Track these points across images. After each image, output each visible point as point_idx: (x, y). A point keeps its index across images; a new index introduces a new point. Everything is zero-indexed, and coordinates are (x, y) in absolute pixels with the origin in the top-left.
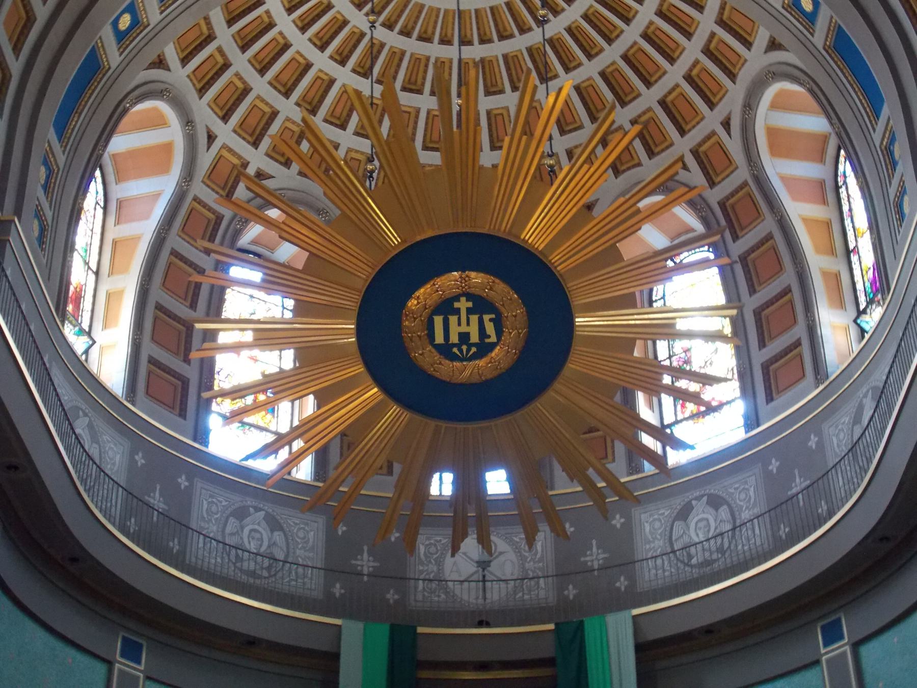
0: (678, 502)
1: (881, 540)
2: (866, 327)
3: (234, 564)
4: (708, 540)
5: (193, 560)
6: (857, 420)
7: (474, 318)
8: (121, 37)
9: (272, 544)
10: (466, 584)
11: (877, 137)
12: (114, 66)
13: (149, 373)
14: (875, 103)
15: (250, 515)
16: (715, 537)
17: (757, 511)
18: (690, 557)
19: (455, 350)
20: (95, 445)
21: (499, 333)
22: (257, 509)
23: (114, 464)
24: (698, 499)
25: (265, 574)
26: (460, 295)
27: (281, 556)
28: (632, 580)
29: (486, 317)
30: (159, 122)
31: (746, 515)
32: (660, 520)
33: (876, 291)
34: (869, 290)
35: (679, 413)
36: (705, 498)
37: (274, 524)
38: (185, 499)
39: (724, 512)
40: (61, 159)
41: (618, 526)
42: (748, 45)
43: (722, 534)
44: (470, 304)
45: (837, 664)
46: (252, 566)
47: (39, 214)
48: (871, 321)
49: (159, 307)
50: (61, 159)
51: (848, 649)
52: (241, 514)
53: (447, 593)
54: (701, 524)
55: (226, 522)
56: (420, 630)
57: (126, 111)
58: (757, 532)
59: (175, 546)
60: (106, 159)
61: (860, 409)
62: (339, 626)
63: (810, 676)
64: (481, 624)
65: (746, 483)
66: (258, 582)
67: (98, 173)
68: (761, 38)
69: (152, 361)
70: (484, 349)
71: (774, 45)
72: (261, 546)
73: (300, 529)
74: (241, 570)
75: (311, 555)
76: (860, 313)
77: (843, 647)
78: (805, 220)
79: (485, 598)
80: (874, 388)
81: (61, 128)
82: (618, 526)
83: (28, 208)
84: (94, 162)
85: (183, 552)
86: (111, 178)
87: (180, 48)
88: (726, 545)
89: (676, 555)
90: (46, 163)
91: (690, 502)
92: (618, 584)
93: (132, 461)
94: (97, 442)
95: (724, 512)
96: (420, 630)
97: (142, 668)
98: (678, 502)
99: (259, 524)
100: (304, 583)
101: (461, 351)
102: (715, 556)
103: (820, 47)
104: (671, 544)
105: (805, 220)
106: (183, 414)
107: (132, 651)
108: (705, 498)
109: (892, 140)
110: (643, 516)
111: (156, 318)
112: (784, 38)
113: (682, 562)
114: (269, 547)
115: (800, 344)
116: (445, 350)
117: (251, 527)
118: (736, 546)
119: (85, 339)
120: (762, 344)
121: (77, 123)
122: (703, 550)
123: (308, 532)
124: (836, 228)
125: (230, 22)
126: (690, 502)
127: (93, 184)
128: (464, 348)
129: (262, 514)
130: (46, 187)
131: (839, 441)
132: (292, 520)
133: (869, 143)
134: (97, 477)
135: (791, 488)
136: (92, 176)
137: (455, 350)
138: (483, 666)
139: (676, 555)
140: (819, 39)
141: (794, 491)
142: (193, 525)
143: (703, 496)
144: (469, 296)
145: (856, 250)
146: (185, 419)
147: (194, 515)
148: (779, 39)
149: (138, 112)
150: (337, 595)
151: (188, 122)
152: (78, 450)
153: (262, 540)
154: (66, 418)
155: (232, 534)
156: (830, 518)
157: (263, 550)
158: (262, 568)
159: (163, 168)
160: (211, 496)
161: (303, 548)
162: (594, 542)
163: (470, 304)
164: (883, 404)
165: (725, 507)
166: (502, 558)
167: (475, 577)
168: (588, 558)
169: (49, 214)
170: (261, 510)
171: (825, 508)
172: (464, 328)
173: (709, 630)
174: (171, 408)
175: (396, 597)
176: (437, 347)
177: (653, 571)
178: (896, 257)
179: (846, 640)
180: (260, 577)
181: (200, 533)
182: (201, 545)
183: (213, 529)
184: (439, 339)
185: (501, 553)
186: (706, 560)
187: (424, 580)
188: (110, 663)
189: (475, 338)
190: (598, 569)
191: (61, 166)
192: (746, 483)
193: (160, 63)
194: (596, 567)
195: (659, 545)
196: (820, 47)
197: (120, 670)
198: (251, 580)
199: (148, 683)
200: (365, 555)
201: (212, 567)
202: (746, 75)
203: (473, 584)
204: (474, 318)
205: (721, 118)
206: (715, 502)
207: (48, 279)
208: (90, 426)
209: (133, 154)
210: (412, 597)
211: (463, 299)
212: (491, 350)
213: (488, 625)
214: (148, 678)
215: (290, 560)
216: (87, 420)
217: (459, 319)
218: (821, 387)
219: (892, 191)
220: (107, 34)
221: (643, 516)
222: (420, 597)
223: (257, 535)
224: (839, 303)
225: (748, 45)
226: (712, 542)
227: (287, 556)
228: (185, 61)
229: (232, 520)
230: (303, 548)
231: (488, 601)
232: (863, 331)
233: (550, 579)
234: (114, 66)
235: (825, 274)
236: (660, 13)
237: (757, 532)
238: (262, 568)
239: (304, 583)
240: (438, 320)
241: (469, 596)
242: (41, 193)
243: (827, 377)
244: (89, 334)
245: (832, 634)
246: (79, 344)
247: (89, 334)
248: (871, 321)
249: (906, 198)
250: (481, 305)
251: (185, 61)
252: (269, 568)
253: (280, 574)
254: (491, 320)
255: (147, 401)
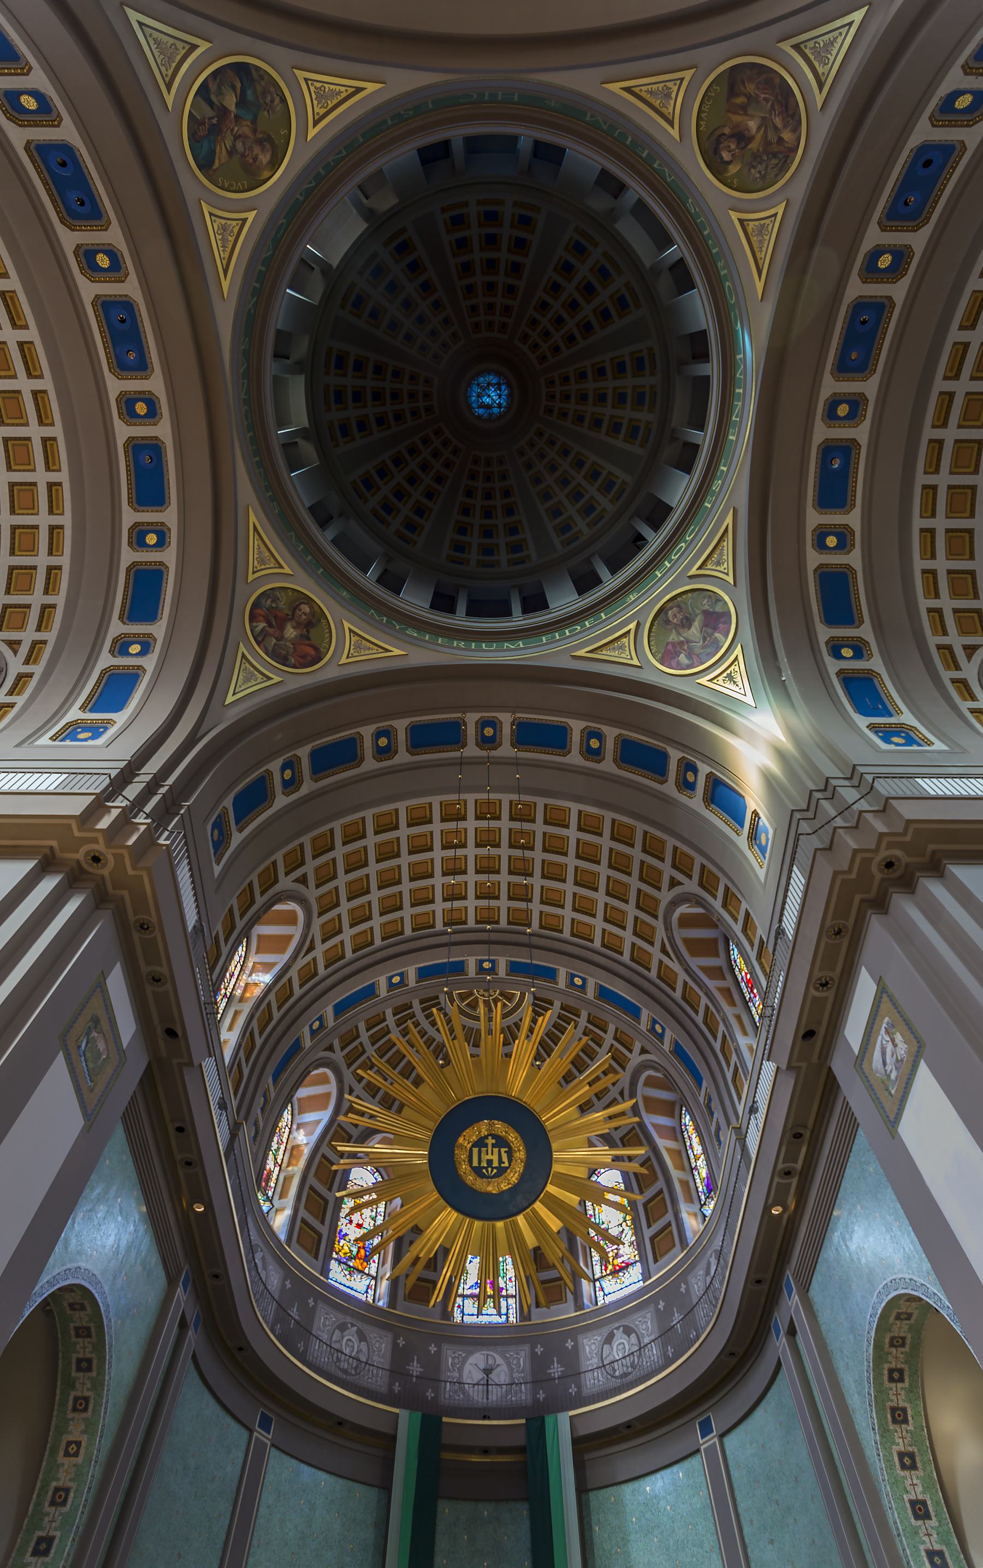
0: (605, 1331)
1: (730, 1354)
2: (707, 1215)
3: (335, 1363)
4: (624, 1358)
5: (311, 1358)
6: (708, 1273)
7: (496, 1150)
8: (313, 1033)
9: (359, 1351)
10: (476, 1386)
11: (701, 1099)
12: (307, 1047)
13: (301, 1228)
14: (698, 1080)
15: (348, 1328)
16: (628, 1355)
17: (653, 1337)
18: (614, 1371)
19: (484, 1171)
20: (264, 1272)
21: (510, 1161)
22: (353, 1325)
23: (273, 1286)
24: (618, 1328)
25: (353, 1372)
26: (488, 1135)
27: (364, 1359)
28: (579, 1387)
29: (503, 1150)
30: (324, 1080)
31: (646, 1340)
32: (594, 1343)
33: (710, 1191)
34: (706, 1191)
35: (604, 1271)
36: (622, 1328)
37: (362, 1337)
38: (310, 1314)
39: (633, 1338)
40: (273, 1095)
41: (570, 1347)
42: (631, 1051)
43: (633, 1353)
44: (494, 1141)
45: (711, 1451)
46: (346, 1367)
47: (256, 1124)
48: (708, 1210)
49: (311, 1188)
50: (273, 1095)
51: (716, 1440)
52: (342, 1328)
53: (464, 1394)
54: (620, 1347)
55: (334, 1332)
56: (445, 1419)
57: (310, 1072)
58: (655, 1352)
59: (301, 1346)
60: (295, 1099)
61: (709, 1264)
62: (398, 1414)
63: (697, 1457)
64: (485, 1418)
65: (646, 1317)
66: (349, 1377)
67: (290, 1105)
68: (637, 1047)
69: (304, 1221)
70: (501, 1171)
71: (644, 1051)
72: (353, 1351)
73: (377, 1341)
74: (339, 1368)
75: (382, 1360)
76: (702, 1206)
77: (713, 1439)
78: (668, 1150)
79: (488, 1399)
80: (716, 1251)
81: (276, 1077)
82: (570, 1347)
83: (251, 1120)
84: (289, 1100)
85: (305, 1351)
86: (296, 1111)
87: (341, 1041)
88: (636, 1362)
89: (605, 1369)
90: (265, 1096)
91: (612, 1331)
92: (570, 1391)
93: (284, 1285)
94: (266, 1270)
95: (633, 1338)
96: (445, 1419)
97: (270, 1437)
98: (605, 1331)
99: (353, 1336)
100: (376, 1381)
101: (487, 1171)
102: (630, 1370)
103: (667, 1051)
104: (603, 1361)
105: (668, 1150)
106: (316, 1257)
107: (265, 1424)
108: (622, 1328)
109: (710, 1100)
110: (585, 1341)
111: (309, 1195)
112: (648, 1047)
113: (610, 1375)
114: (357, 1352)
115: (671, 1225)
116: (478, 1171)
117: (347, 1338)
118: (643, 1362)
119: (268, 1204)
120: (649, 1226)
121: (284, 1076)
122: (623, 1365)
123: (382, 1344)
124: (684, 1155)
125: (368, 1030)
126: (612, 1331)
127: (286, 1112)
128: (490, 1169)
129: (356, 1328)
130: (262, 1109)
131: (699, 1287)
132: (373, 1333)
133: (697, 1101)
134: (262, 1293)
135: (673, 1321)
136: (286, 1107)
137: (484, 1171)
138: (486, 1451)
139: (605, 1369)
140: (666, 1047)
141: (675, 1323)
142: (314, 1333)
143: (620, 1326)
144: (494, 1136)
145: (696, 1168)
146: (317, 1260)
147: (315, 1326)
148: (646, 1048)
149: (314, 1075)
150: (396, 1391)
151: (340, 1081)
152: (254, 1273)
153: (353, 1347)
154: (251, 1249)
155: (336, 1342)
156: (698, 1339)
157: (353, 1355)
158: (352, 1368)
159: (325, 1107)
160: (327, 1314)
161: (378, 1355)
162: (555, 1359)
163: (494, 1141)
164: (722, 1261)
165: (634, 1334)
166: (499, 1369)
167: (482, 1382)
168: (551, 1371)
169: (261, 1124)
170: (355, 1326)
171: (695, 1333)
172: (489, 1157)
173: (628, 1425)
174: (309, 1252)
175: (433, 1395)
176: (474, 1169)
177: (592, 1381)
178: (719, 1167)
179: (715, 1433)
180: (350, 1374)
181: (318, 1338)
182: (317, 1348)
183: (325, 1337)
184: (475, 1163)
185: (498, 1365)
186: (625, 1373)
187: (450, 1382)
188: (251, 1431)
189: (496, 1164)
190: (558, 1378)
191: (272, 1098)
192: (646, 1317)
193: (330, 1048)
194: (557, 1376)
195: (595, 1362)
196: (667, 1051)
197: (256, 1437)
198: (345, 1376)
199: (273, 1449)
200: (415, 1363)
201: (322, 1364)
202: (631, 1066)
203: (481, 1387)
204: (496, 1150)
205: (619, 1091)
206: (628, 1331)
207: (254, 1162)
208: (263, 1259)
209: (310, 1098)
210: (442, 1396)
211: (490, 1137)
212: (506, 1171)
213: (488, 1418)
214: (273, 1445)
215: (370, 1362)
216: (262, 1253)
217: (487, 1151)
218: (685, 1252)
219: (713, 1129)
220: (306, 1030)
221: (585, 1341)
222: (447, 1396)
223: (351, 1344)
224: (689, 1199)
225: (631, 1051)
226: (628, 1358)
227: (367, 1360)
228: (342, 1049)
229: (337, 1331)
230: (378, 1355)
231: (490, 1401)
232: (705, 1216)
233: (528, 1385)
234: (307, 1047)
235: (681, 1182)
236: (589, 1021)
237: (655, 1352)
238: (352, 1368)
239: (376, 1381)
240: (475, 1150)
241: (477, 1395)
242: (259, 1111)
243: (688, 1246)
244: (271, 1201)
245: (706, 1429)
246: (265, 1207)
247: (271, 1201)
248: (708, 1210)
249: (721, 1132)
250: (501, 1142)
251: (342, 1049)
252: (356, 1369)
253: (362, 1373)
254: (505, 1152)
255: (298, 1246)
